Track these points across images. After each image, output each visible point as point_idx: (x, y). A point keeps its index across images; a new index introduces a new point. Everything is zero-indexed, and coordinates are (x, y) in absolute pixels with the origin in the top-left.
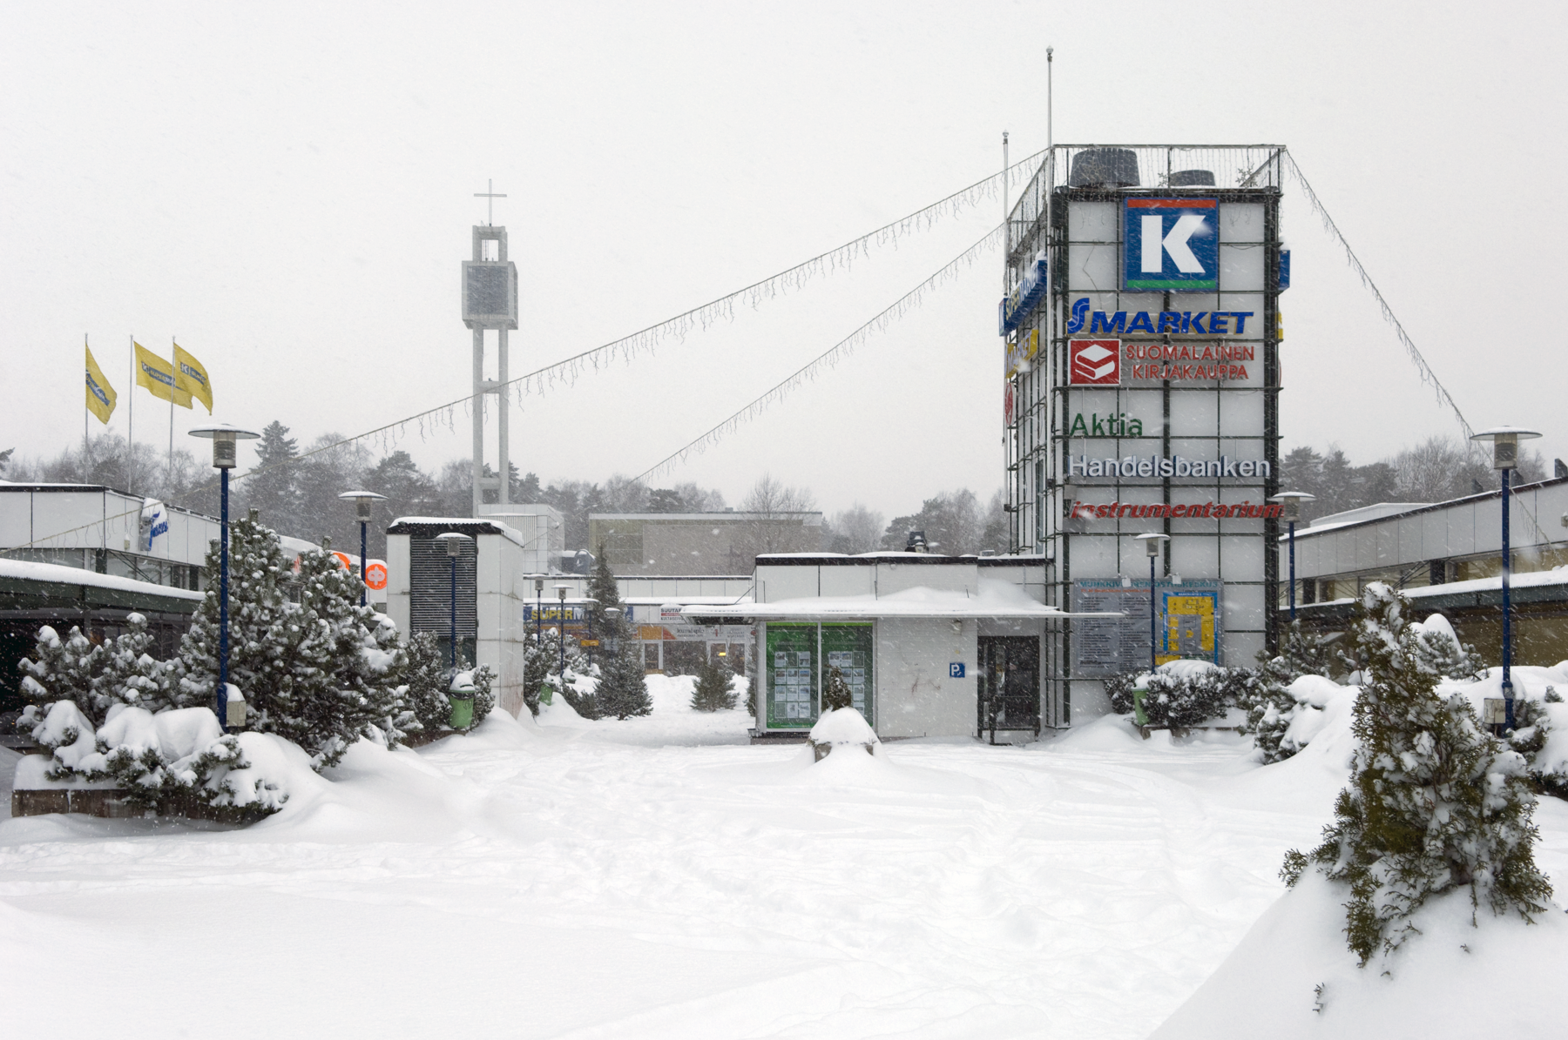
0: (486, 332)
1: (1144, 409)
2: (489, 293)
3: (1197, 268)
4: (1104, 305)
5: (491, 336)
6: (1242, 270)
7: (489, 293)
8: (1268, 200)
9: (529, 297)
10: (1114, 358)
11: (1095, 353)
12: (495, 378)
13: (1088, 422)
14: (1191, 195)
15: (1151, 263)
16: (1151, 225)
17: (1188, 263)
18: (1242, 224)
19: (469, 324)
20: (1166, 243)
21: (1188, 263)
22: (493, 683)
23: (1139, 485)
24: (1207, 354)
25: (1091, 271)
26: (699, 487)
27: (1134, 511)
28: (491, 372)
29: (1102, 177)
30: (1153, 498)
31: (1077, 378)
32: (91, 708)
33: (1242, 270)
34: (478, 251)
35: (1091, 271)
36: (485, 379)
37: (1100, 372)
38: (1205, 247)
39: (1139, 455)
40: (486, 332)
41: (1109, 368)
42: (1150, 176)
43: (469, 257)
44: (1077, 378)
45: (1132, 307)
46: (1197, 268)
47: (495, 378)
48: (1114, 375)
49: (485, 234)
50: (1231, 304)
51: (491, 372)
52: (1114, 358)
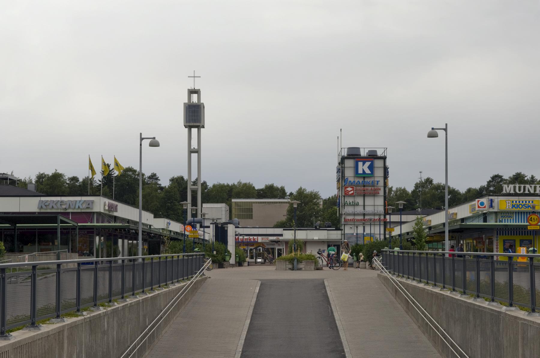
0: (192, 129)
1: (360, 200)
2: (194, 115)
3: (370, 172)
4: (351, 179)
5: (194, 131)
6: (379, 173)
7: (194, 115)
8: (384, 158)
9: (209, 116)
10: (353, 190)
11: (349, 189)
12: (196, 147)
13: (348, 202)
14: (372, 156)
15: (360, 171)
16: (360, 164)
17: (368, 171)
18: (378, 163)
19: (186, 127)
20: (363, 167)
21: (368, 171)
22: (532, 236)
23: (358, 215)
24: (371, 189)
25: (349, 173)
26: (275, 185)
27: (358, 220)
28: (194, 145)
29: (353, 155)
30: (362, 217)
31: (346, 194)
32: (413, 244)
33: (379, 173)
34: (189, 98)
35: (349, 173)
36: (192, 148)
37: (350, 193)
38: (371, 168)
39: (359, 209)
40: (192, 129)
41: (352, 192)
42: (363, 153)
43: (186, 101)
44: (346, 194)
45: (357, 180)
46: (370, 172)
47: (196, 147)
48: (353, 194)
49: (192, 92)
50: (376, 179)
51: (194, 145)
52: (353, 190)
